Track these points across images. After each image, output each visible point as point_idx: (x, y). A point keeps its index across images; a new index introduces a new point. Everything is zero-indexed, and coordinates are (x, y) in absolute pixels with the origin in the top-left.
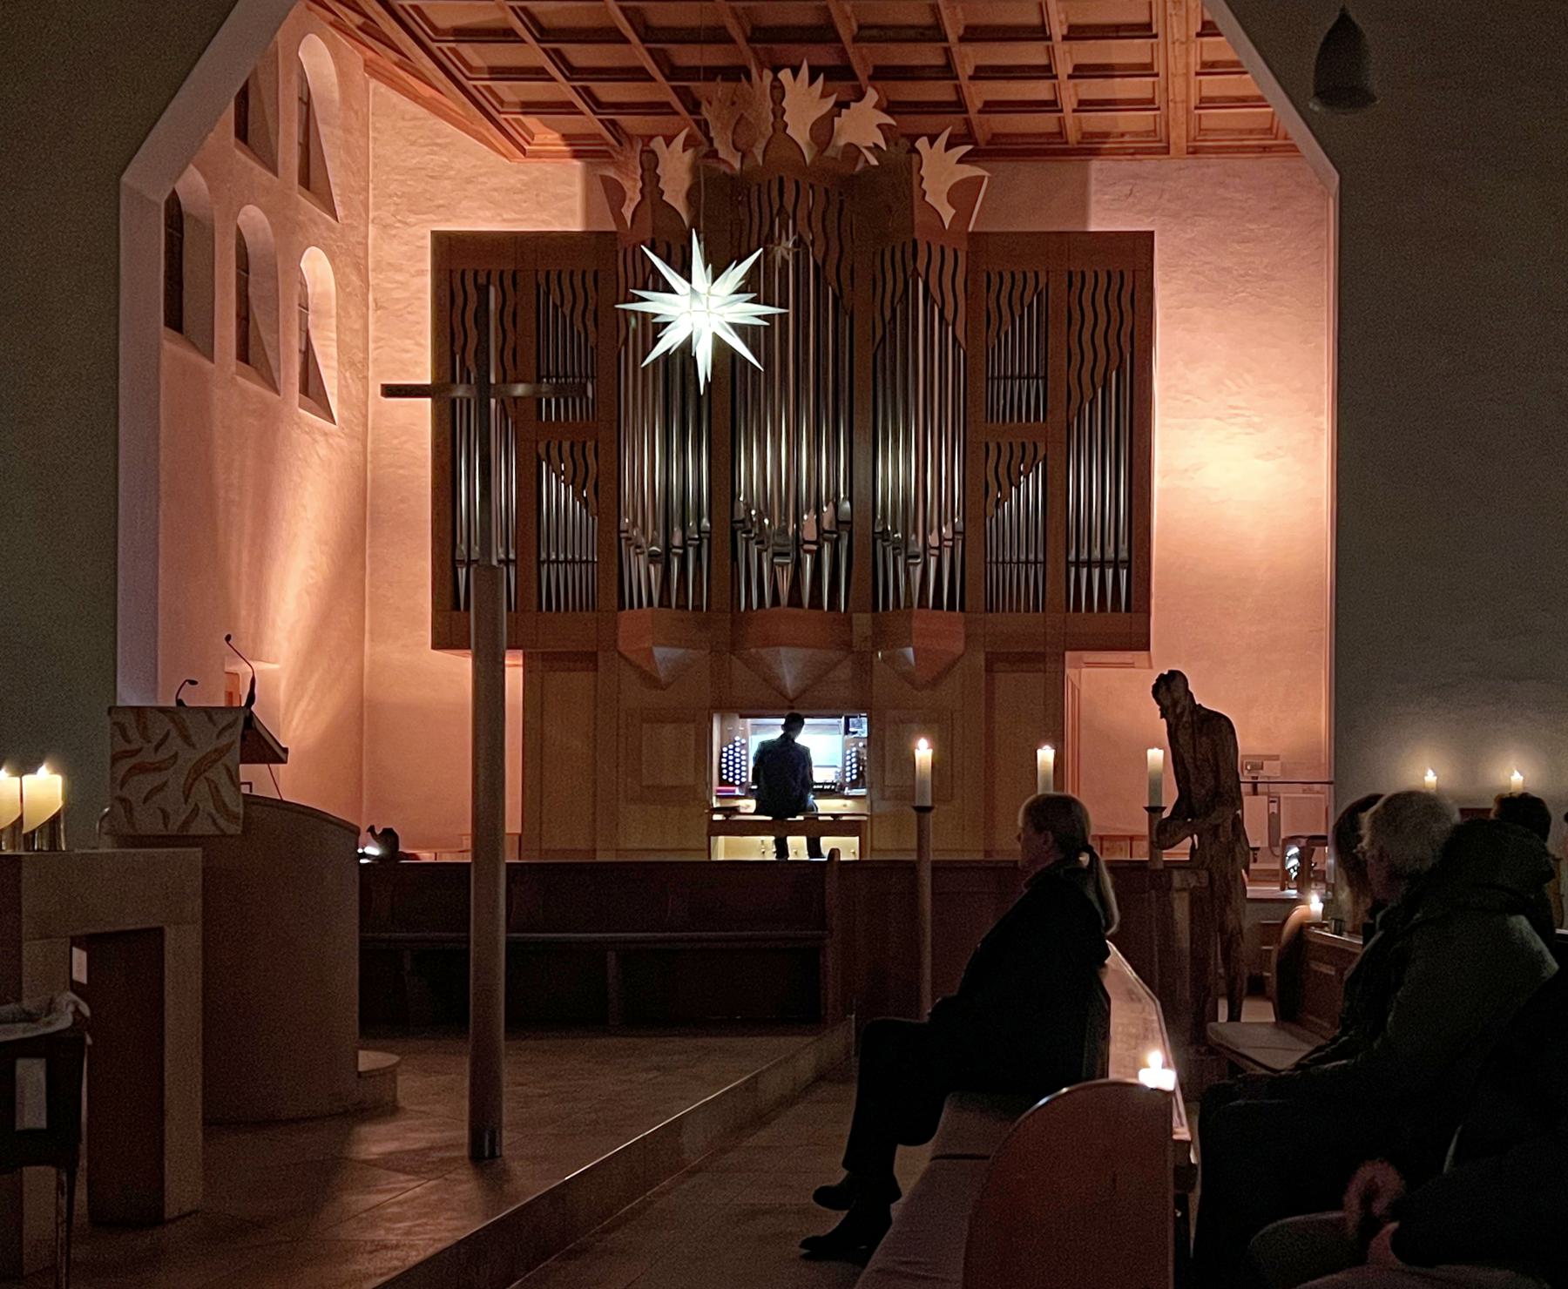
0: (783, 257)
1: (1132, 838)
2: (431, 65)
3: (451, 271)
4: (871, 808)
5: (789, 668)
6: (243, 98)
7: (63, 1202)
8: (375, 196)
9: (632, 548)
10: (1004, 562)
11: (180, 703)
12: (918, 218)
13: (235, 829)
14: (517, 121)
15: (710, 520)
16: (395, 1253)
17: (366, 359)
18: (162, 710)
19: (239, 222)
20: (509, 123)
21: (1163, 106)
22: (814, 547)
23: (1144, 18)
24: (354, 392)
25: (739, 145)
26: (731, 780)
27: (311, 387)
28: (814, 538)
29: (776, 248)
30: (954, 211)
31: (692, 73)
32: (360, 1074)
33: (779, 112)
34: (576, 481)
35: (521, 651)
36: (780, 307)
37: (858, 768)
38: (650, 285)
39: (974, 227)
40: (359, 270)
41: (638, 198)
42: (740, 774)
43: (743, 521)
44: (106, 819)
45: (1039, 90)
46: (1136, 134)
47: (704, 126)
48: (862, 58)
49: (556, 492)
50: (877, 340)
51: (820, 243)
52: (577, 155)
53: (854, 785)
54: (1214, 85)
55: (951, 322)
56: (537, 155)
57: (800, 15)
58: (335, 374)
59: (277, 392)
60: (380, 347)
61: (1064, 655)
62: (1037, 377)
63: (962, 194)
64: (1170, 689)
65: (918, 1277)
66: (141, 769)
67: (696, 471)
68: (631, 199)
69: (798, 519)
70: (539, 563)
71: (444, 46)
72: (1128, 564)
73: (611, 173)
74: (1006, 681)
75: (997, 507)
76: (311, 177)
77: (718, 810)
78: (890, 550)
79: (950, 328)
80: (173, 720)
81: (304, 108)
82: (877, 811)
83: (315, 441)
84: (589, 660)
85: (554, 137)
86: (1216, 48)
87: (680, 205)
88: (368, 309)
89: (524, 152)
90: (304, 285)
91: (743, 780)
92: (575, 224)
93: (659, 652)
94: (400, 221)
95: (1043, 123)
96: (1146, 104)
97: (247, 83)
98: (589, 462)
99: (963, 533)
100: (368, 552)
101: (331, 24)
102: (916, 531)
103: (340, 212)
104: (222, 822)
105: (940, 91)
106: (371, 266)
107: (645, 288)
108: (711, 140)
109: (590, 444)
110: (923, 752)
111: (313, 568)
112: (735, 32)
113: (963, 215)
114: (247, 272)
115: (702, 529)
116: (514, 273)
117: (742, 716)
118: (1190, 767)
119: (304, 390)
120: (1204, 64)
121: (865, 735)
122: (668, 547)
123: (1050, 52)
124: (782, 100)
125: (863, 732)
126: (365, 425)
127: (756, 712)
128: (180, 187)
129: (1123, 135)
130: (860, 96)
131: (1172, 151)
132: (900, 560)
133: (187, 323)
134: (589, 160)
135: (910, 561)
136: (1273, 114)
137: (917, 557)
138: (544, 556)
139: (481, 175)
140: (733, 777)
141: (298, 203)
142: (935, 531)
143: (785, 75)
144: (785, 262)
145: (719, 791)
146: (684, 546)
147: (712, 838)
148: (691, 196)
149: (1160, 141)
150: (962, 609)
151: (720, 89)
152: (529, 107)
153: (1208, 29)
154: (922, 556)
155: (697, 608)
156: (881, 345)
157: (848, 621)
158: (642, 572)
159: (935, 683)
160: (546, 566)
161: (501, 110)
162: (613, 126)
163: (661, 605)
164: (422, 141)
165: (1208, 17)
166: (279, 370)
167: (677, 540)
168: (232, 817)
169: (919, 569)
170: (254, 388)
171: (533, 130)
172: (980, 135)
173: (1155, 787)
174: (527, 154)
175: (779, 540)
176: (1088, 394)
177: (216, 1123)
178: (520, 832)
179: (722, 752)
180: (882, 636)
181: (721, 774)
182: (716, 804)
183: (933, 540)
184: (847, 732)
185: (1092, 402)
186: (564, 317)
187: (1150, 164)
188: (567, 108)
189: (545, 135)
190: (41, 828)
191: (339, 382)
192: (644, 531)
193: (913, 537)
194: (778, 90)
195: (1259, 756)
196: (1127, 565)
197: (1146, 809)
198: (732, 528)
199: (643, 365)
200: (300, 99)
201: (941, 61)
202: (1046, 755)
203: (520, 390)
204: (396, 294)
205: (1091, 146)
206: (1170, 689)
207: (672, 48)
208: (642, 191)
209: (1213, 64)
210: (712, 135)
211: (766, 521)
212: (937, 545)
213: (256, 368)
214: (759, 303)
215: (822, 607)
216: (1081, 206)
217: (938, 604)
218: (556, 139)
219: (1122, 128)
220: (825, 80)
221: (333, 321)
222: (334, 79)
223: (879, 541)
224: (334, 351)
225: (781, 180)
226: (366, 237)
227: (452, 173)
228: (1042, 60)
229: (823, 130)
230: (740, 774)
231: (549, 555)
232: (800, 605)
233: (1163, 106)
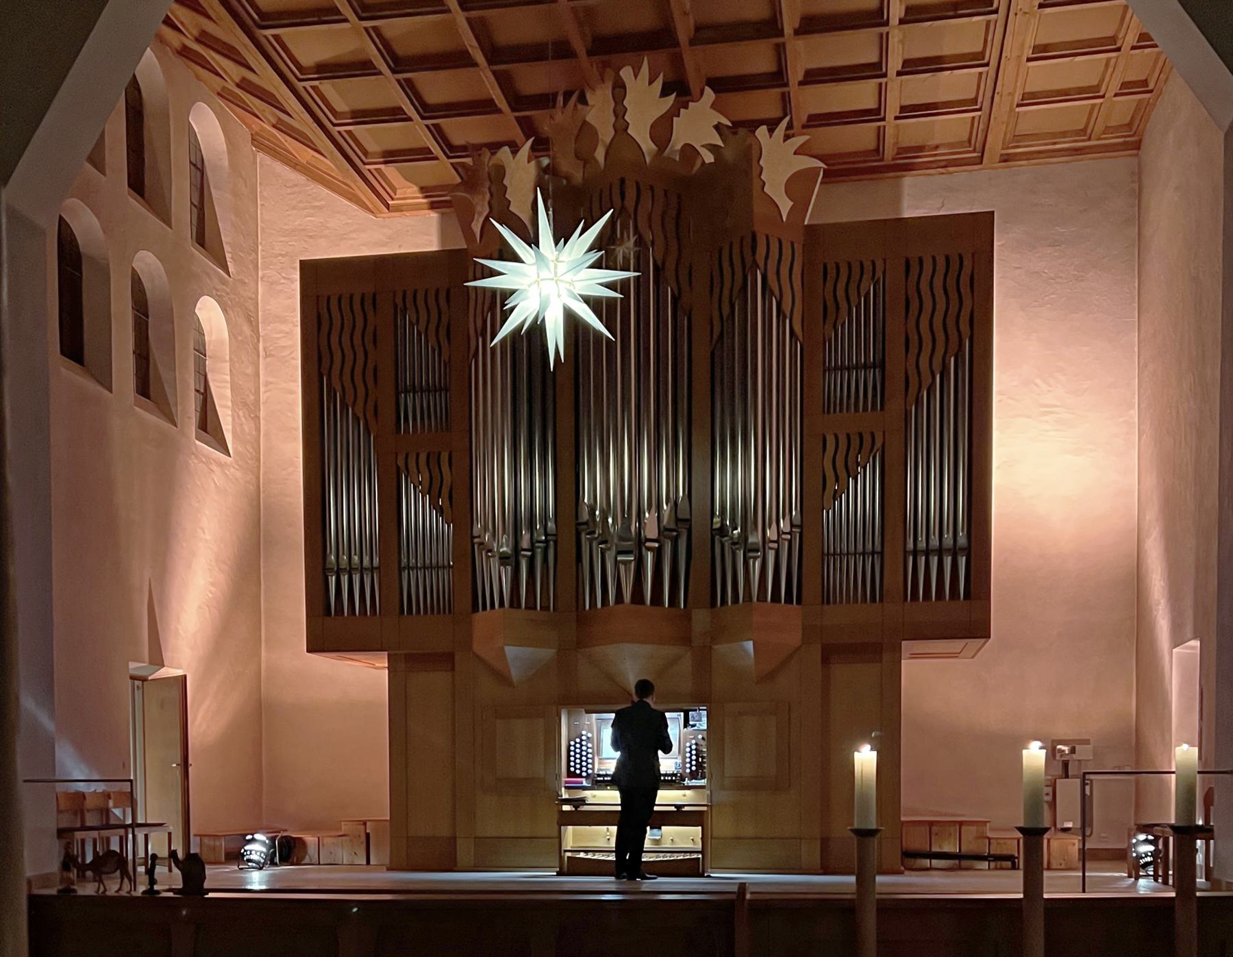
1: (961, 823)
3: (318, 297)
4: (711, 797)
8: (263, 257)
9: (484, 553)
17: (257, 401)
19: (134, 265)
20: (371, 173)
26: (578, 772)
27: (208, 425)
29: (618, 249)
30: (792, 203)
34: (432, 490)
35: (386, 653)
36: (634, 271)
37: (697, 760)
39: (809, 220)
40: (251, 322)
42: (586, 766)
43: (586, 523)
46: (951, 145)
50: (715, 336)
51: (660, 242)
52: (433, 206)
53: (693, 775)
55: (788, 316)
56: (398, 209)
57: (641, 19)
60: (269, 391)
61: (901, 643)
62: (874, 366)
70: (400, 570)
71: (307, 84)
74: (842, 672)
77: (567, 802)
79: (788, 321)
81: (199, 174)
84: (446, 660)
88: (259, 356)
89: (387, 206)
91: (590, 771)
93: (510, 651)
94: (284, 278)
98: (444, 471)
99: (801, 526)
103: (231, 269)
109: (445, 457)
111: (212, 584)
112: (579, 46)
113: (800, 206)
115: (549, 532)
116: (374, 295)
117: (588, 712)
126: (258, 460)
129: (937, 147)
134: (444, 210)
135: (751, 554)
137: (757, 551)
139: (351, 232)
140: (580, 769)
141: (192, 255)
142: (774, 524)
145: (566, 782)
147: (562, 827)
149: (974, 151)
150: (799, 602)
152: (391, 156)
154: (761, 549)
156: (719, 345)
157: (687, 616)
159: (771, 676)
160: (406, 571)
161: (366, 160)
163: (511, 605)
164: (301, 205)
167: (525, 543)
170: (153, 419)
171: (395, 184)
174: (391, 208)
176: (927, 380)
179: (570, 746)
180: (718, 633)
181: (569, 766)
182: (565, 796)
183: (771, 534)
184: (686, 724)
186: (419, 334)
188: (424, 154)
191: (233, 419)
196: (966, 551)
198: (577, 529)
199: (492, 345)
204: (283, 343)
212: (776, 538)
213: (155, 403)
217: (776, 597)
218: (414, 193)
221: (227, 366)
223: (717, 537)
224: (228, 393)
227: (327, 232)
229: (662, 130)
230: (586, 766)
232: (642, 602)
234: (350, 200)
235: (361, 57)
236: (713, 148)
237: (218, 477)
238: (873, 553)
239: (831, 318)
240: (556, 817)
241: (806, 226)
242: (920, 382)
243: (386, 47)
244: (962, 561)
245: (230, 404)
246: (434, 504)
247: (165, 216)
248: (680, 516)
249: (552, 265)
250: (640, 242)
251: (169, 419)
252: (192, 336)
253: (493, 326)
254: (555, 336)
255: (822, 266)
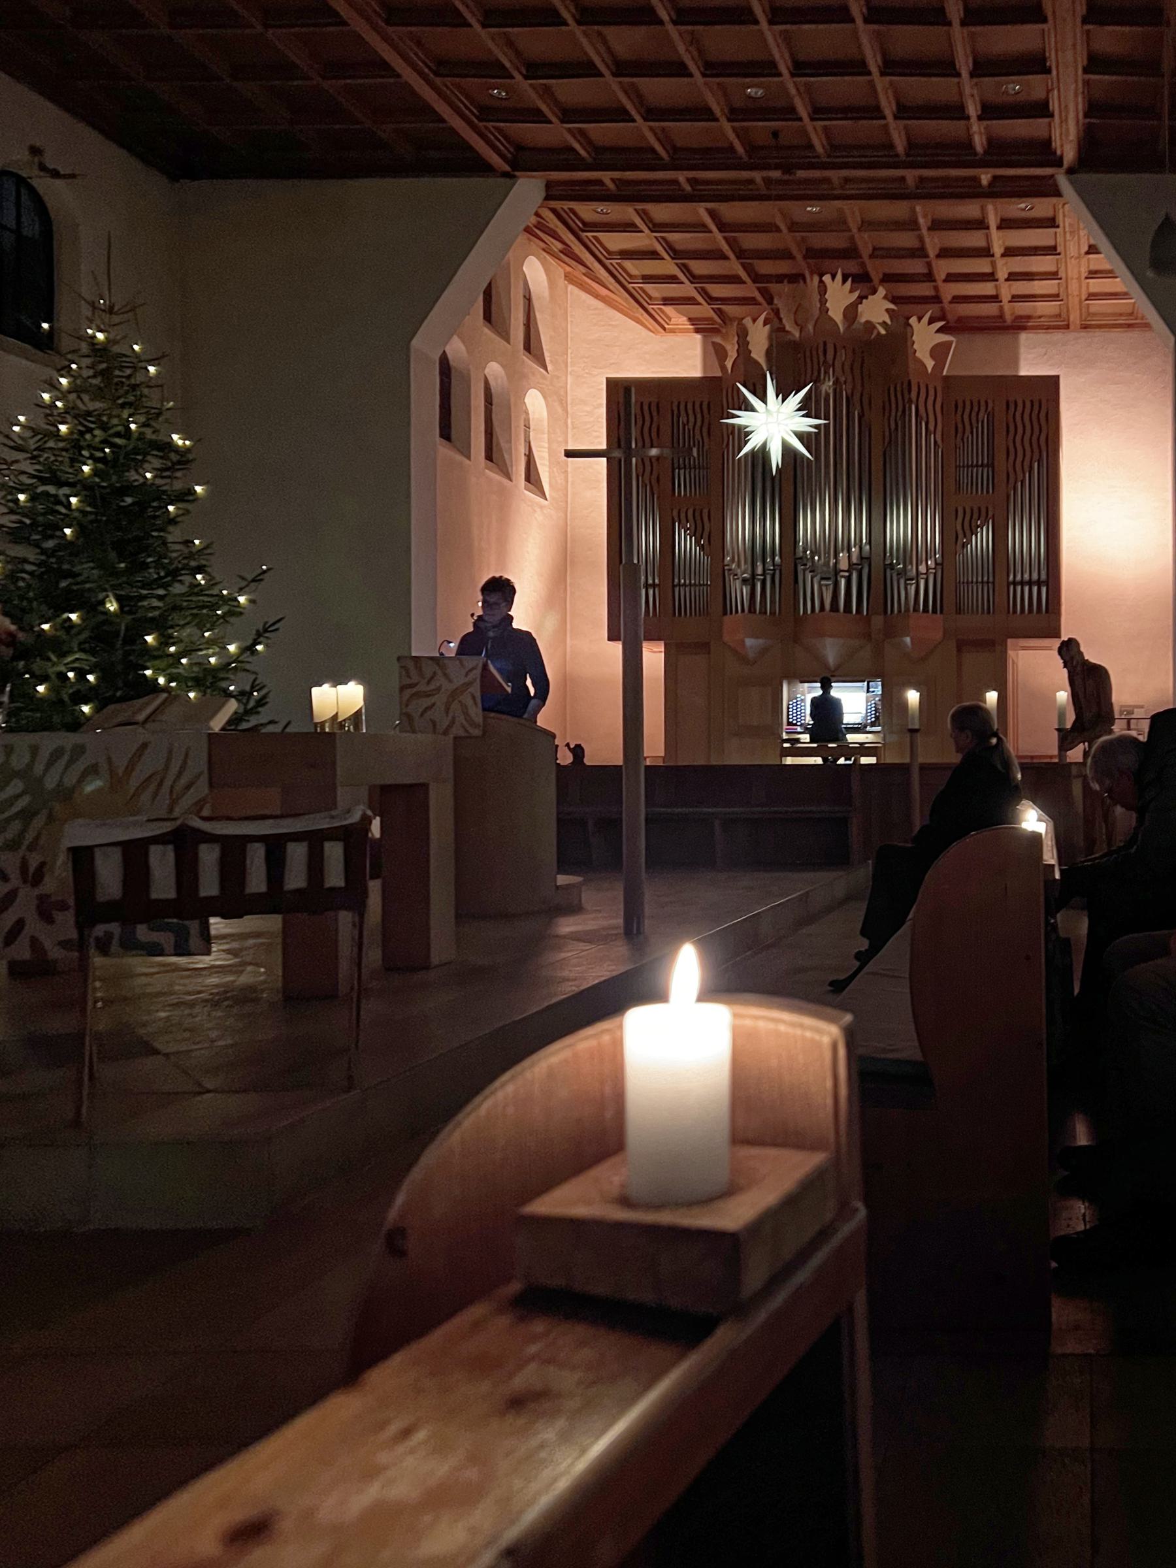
0: (826, 392)
2: (606, 274)
4: (884, 739)
5: (831, 650)
6: (488, 294)
7: (356, 932)
10: (967, 583)
11: (442, 654)
12: (911, 365)
13: (477, 732)
14: (660, 309)
15: (781, 557)
16: (573, 983)
18: (432, 658)
21: (1065, 298)
22: (847, 574)
23: (1052, 243)
24: (559, 481)
25: (799, 322)
27: (532, 476)
28: (846, 568)
31: (768, 278)
32: (557, 887)
33: (823, 302)
34: (697, 533)
38: (743, 408)
41: (735, 355)
43: (801, 558)
44: (398, 728)
45: (987, 288)
46: (1050, 317)
47: (777, 312)
48: (876, 269)
49: (685, 543)
51: (850, 386)
52: (697, 331)
53: (873, 724)
54: (1096, 285)
56: (673, 331)
58: (547, 469)
59: (511, 481)
62: (988, 466)
63: (939, 352)
64: (1069, 650)
65: (895, 977)
66: (417, 695)
67: (773, 530)
68: (731, 356)
69: (836, 556)
70: (674, 586)
71: (614, 262)
72: (1047, 583)
73: (718, 340)
75: (963, 547)
76: (531, 345)
77: (787, 741)
78: (895, 578)
80: (438, 664)
82: (887, 741)
83: (535, 511)
84: (703, 647)
85: (684, 320)
86: (1098, 262)
87: (762, 361)
89: (664, 329)
90: (527, 414)
92: (696, 372)
95: (989, 309)
96: (1055, 297)
97: (490, 284)
99: (942, 564)
100: (568, 581)
101: (544, 250)
102: (911, 563)
103: (550, 367)
104: (471, 730)
105: (924, 290)
106: (569, 402)
107: (740, 409)
108: (780, 320)
109: (705, 511)
110: (913, 697)
113: (939, 365)
114: (491, 404)
117: (802, 682)
118: (1083, 700)
119: (528, 479)
120: (1091, 272)
121: (880, 693)
122: (754, 575)
123: (993, 264)
124: (825, 293)
125: (879, 690)
126: (567, 502)
127: (811, 679)
128: (448, 349)
130: (874, 292)
131: (1072, 327)
132: (902, 582)
133: (454, 436)
136: (1134, 303)
137: (912, 579)
138: (676, 581)
141: (523, 361)
142: (924, 563)
143: (827, 278)
144: (827, 395)
146: (764, 574)
148: (768, 353)
151: (786, 287)
152: (667, 301)
153: (1092, 250)
155: (773, 613)
158: (740, 592)
162: (719, 312)
163: (750, 611)
165: (1092, 242)
166: (512, 466)
167: (759, 570)
168: (476, 726)
169: (913, 587)
170: (497, 477)
172: (949, 317)
173: (1062, 716)
175: (825, 569)
176: (1020, 477)
177: (461, 917)
178: (663, 754)
180: (891, 632)
181: (788, 719)
182: (785, 736)
183: (922, 569)
184: (868, 691)
185: (1023, 482)
186: (689, 430)
187: (1058, 336)
188: (690, 301)
189: (677, 318)
190: (349, 718)
192: (739, 565)
193: (910, 567)
194: (823, 289)
195: (1130, 706)
197: (1057, 729)
200: (525, 296)
201: (925, 271)
202: (992, 697)
203: (654, 452)
205: (1021, 324)
206: (1069, 650)
207: (755, 262)
208: (738, 350)
209: (1096, 272)
210: (782, 316)
211: (816, 558)
214: (811, 417)
215: (851, 612)
216: (1015, 362)
217: (926, 610)
219: (1039, 313)
220: (853, 282)
221: (546, 436)
222: (546, 283)
224: (546, 455)
225: (825, 344)
226: (566, 383)
228: (988, 270)
229: (851, 313)
231: (679, 581)
233: (1065, 298)
234: (638, 323)
235: (651, 249)
236: (884, 324)
237: (539, 516)
238: (988, 582)
239: (960, 435)
240: (778, 752)
241: (947, 377)
242: (1016, 478)
243: (638, 97)
244: (1044, 590)
245: (547, 463)
246: (697, 543)
247: (505, 335)
248: (864, 555)
249: (775, 415)
250: (836, 382)
251: (502, 471)
252: (524, 416)
253: (739, 444)
254: (776, 457)
255: (954, 402)
